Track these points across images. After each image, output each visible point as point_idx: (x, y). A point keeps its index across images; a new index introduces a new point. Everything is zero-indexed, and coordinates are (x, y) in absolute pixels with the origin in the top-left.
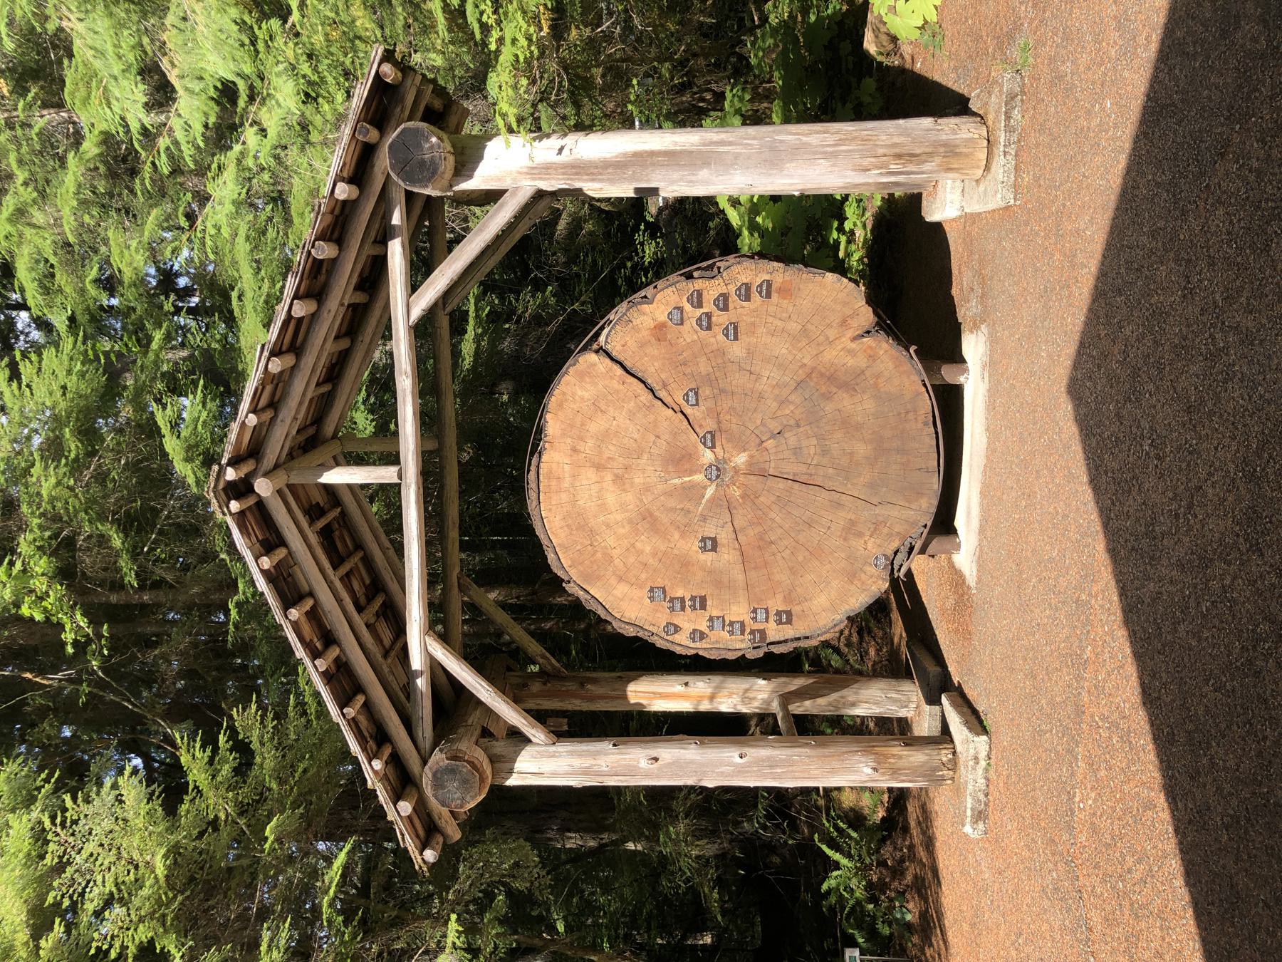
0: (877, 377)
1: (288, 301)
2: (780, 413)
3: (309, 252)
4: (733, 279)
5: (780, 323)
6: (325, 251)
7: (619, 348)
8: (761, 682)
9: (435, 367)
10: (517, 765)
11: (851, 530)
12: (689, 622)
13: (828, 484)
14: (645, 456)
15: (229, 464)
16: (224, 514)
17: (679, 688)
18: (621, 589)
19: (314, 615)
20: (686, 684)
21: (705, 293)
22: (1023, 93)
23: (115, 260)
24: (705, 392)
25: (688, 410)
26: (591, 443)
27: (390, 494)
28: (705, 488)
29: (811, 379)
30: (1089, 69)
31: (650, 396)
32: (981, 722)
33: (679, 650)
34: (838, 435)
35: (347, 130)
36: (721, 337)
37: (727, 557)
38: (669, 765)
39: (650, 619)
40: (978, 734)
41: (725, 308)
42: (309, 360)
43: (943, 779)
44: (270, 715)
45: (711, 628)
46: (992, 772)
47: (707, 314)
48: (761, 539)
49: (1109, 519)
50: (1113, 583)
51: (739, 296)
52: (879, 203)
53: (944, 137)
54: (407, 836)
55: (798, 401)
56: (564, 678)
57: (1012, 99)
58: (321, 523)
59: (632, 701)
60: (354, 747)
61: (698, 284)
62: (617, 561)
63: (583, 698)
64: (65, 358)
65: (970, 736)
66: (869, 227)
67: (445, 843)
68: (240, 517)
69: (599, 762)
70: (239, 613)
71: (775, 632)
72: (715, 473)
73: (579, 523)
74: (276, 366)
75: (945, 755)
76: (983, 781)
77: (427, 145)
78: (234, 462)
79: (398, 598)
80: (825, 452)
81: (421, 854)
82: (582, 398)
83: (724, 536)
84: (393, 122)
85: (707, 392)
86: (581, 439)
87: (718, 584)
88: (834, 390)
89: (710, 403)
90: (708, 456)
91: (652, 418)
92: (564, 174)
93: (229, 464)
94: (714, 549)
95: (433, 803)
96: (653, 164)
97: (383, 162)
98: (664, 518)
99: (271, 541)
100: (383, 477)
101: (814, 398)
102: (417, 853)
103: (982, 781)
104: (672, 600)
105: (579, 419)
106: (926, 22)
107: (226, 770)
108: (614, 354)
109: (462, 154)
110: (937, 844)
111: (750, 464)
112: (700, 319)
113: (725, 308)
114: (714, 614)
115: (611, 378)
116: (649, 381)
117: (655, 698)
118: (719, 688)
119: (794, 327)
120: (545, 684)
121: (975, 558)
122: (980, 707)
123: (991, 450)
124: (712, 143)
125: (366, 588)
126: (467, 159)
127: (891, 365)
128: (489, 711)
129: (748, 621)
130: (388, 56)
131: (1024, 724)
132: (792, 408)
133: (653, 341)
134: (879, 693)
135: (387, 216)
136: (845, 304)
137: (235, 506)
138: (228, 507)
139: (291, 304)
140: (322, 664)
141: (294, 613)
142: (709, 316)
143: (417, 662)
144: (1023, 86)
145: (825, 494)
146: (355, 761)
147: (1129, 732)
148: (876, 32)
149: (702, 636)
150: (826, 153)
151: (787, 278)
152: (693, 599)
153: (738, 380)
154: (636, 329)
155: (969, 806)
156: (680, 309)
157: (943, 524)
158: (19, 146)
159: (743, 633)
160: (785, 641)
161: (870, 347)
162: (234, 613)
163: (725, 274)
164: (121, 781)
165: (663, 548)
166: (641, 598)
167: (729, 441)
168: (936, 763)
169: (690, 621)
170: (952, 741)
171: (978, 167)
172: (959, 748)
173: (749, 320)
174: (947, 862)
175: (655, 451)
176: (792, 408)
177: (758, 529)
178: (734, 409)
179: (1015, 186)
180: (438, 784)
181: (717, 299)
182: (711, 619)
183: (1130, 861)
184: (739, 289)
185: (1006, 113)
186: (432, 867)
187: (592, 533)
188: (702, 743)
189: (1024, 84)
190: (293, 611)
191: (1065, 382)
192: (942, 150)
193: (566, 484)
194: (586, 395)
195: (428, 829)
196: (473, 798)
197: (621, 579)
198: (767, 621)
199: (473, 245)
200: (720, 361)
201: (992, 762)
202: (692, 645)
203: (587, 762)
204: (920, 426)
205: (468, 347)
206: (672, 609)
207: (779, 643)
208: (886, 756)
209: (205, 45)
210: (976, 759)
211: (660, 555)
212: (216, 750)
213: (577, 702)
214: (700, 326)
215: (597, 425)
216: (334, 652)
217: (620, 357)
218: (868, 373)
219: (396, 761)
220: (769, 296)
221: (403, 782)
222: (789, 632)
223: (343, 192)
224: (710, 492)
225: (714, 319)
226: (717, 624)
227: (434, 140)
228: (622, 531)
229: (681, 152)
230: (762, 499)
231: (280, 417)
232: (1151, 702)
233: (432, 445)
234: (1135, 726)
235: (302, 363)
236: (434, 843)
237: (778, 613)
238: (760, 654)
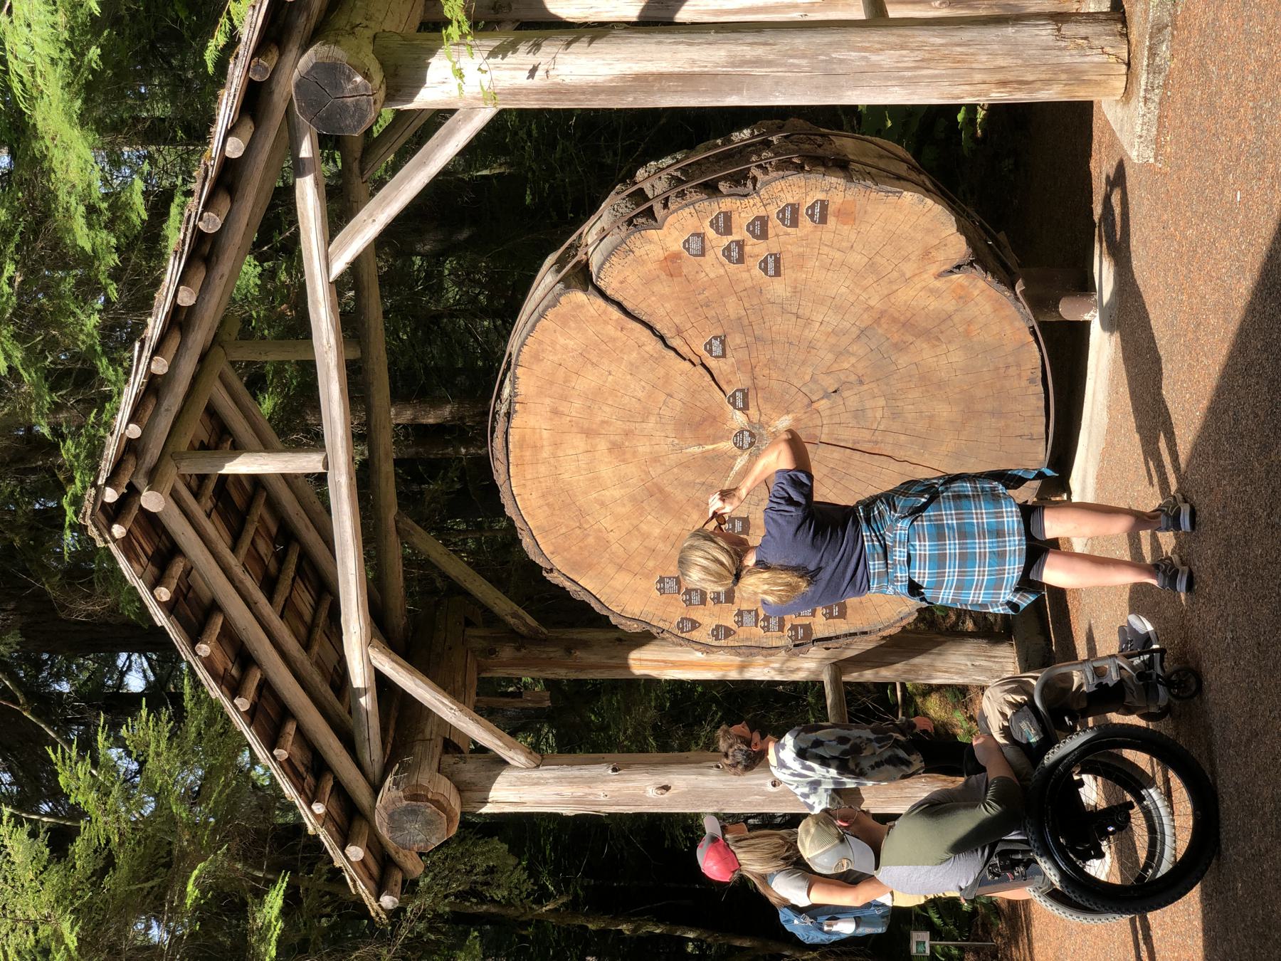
0: (970, 323)
1: (172, 289)
4: (773, 198)
5: (838, 255)
7: (615, 284)
9: (357, 298)
10: (492, 794)
13: (899, 454)
14: (653, 419)
16: (106, 541)
18: (622, 580)
21: (735, 217)
22: (1175, 27)
24: (735, 340)
25: (711, 363)
26: (578, 404)
28: (734, 458)
29: (879, 325)
31: (660, 345)
34: (915, 394)
36: (757, 272)
38: (684, 794)
39: (659, 613)
41: (764, 235)
44: (164, 718)
45: (740, 623)
47: (738, 243)
51: (782, 220)
53: (1068, 60)
54: (359, 882)
55: (861, 352)
56: (545, 641)
57: (1160, 30)
61: (726, 204)
62: (615, 547)
63: (568, 667)
69: (594, 791)
72: (747, 440)
73: (561, 499)
77: (350, 86)
80: (896, 415)
81: (377, 900)
82: (565, 348)
86: (564, 398)
88: (910, 339)
91: (661, 372)
98: (679, 495)
101: (883, 349)
104: (688, 592)
105: (561, 373)
108: (608, 292)
109: (396, 75)
112: (728, 248)
113: (764, 235)
114: (745, 607)
115: (606, 323)
116: (658, 327)
119: (857, 259)
120: (518, 649)
124: (744, 63)
126: (403, 75)
127: (988, 308)
132: (853, 360)
133: (663, 276)
135: (294, 147)
136: (929, 231)
139: (177, 291)
142: (740, 245)
143: (359, 677)
144: (1174, 17)
146: (292, 807)
150: (902, 78)
151: (849, 198)
153: (781, 325)
154: (640, 261)
156: (701, 236)
159: (781, 628)
160: (837, 637)
161: (961, 286)
167: (766, 400)
169: (712, 615)
173: (795, 250)
176: (853, 360)
179: (1156, 141)
181: (753, 223)
184: (783, 211)
185: (1150, 48)
187: (582, 513)
192: (1064, 76)
193: (546, 453)
194: (571, 344)
197: (620, 568)
200: (755, 301)
204: (1024, 383)
206: (689, 603)
211: (673, 538)
214: (729, 257)
215: (587, 381)
218: (956, 318)
220: (823, 220)
221: (350, 818)
223: (237, 148)
225: (747, 249)
226: (748, 619)
228: (621, 510)
229: (701, 74)
235: (190, 343)
236: (391, 884)
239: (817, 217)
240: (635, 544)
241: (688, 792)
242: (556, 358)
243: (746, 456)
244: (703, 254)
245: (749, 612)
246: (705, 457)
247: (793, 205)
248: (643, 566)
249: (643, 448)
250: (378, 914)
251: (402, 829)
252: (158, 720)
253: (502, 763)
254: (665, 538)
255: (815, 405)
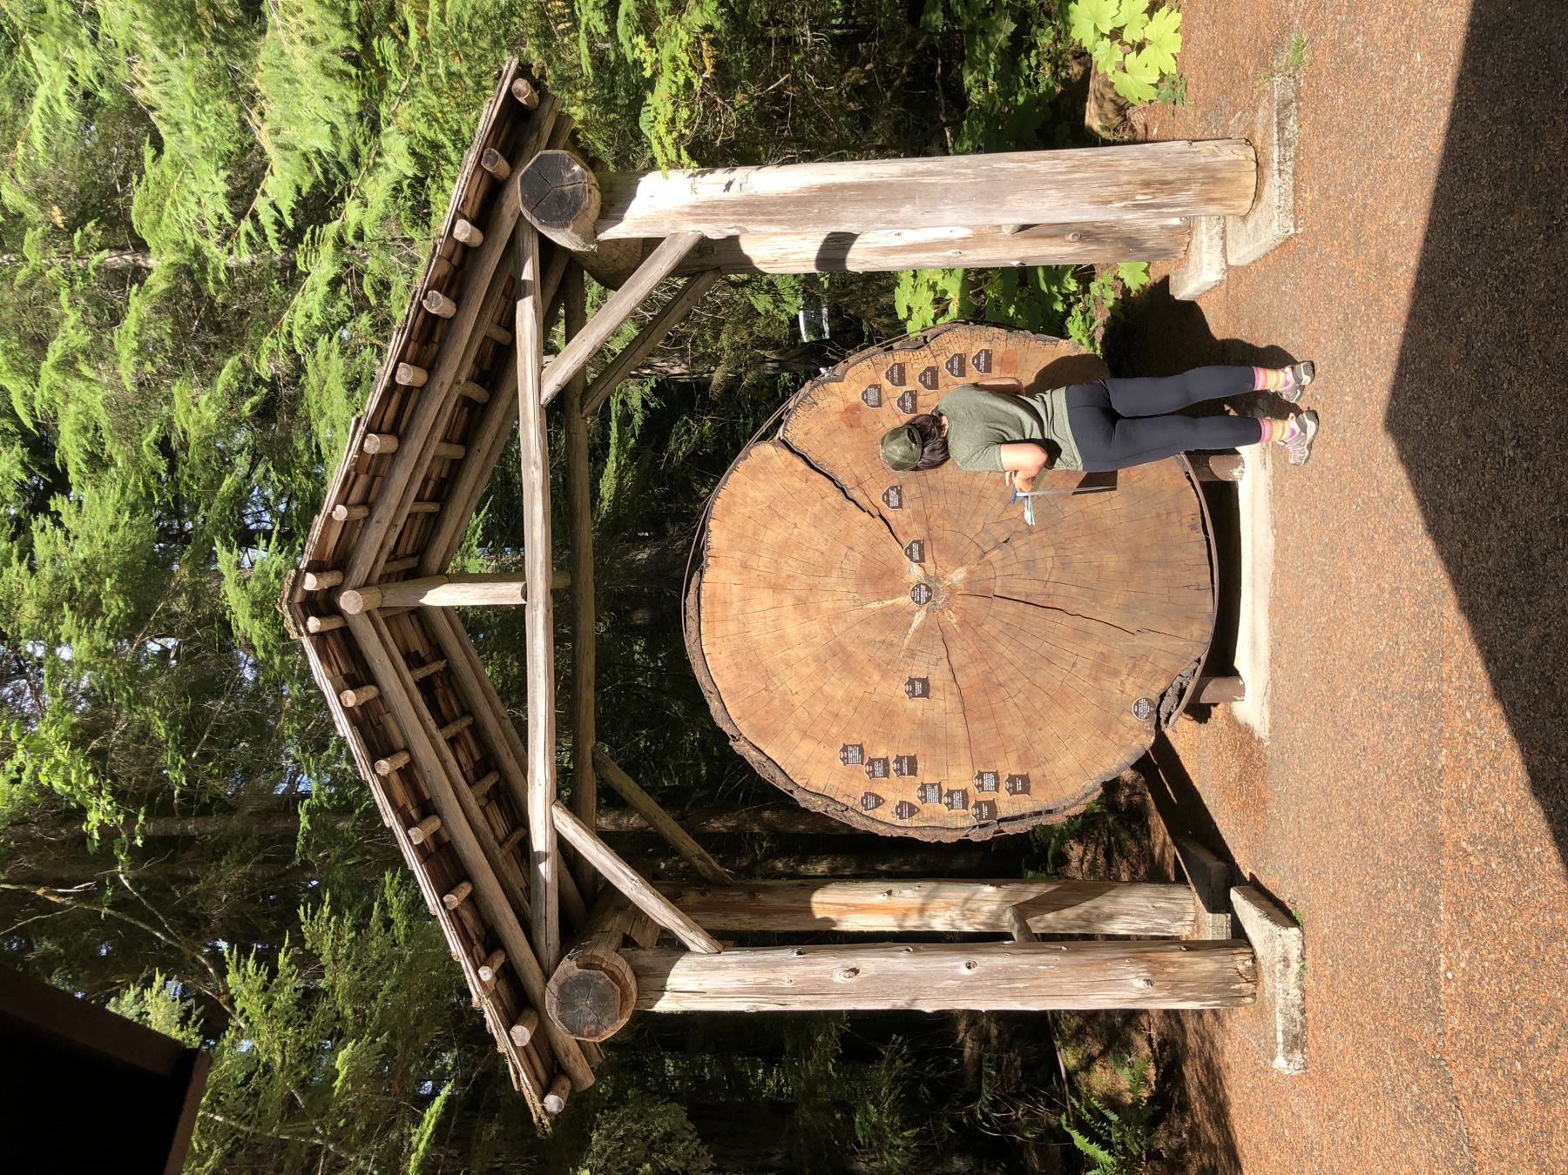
1: (392, 363)
2: (1006, 516)
3: (420, 304)
4: (942, 349)
6: (439, 305)
7: (800, 436)
8: (989, 889)
10: (670, 980)
11: (1103, 666)
12: (895, 791)
13: (1072, 608)
14: (835, 574)
15: (308, 569)
16: (300, 634)
17: (880, 899)
18: (806, 748)
19: (408, 774)
20: (889, 893)
21: (908, 368)
23: (180, 420)
25: (890, 514)
26: (766, 558)
27: (513, 618)
28: (912, 614)
30: (1388, 30)
31: (841, 497)
32: (1288, 913)
33: (882, 831)
34: (1082, 544)
35: (471, 157)
37: (941, 705)
39: (843, 787)
40: (1287, 927)
41: (934, 385)
42: (414, 445)
43: (1240, 995)
44: (348, 923)
45: (924, 799)
46: (1308, 977)
48: (987, 680)
49: (1460, 568)
50: (1474, 650)
51: (951, 370)
52: (1111, 303)
53: (1202, 160)
54: (523, 1075)
56: (730, 887)
58: (422, 673)
59: (818, 916)
60: (456, 948)
61: (899, 357)
63: (753, 912)
64: (111, 510)
65: (1276, 929)
66: (1099, 337)
67: (572, 1090)
68: (320, 639)
69: (780, 975)
70: (310, 821)
71: (1007, 804)
72: (924, 594)
74: (374, 444)
75: (1242, 962)
76: (1297, 992)
78: (316, 567)
79: (515, 775)
80: (1066, 565)
81: (542, 1100)
82: (755, 501)
83: (939, 676)
84: (527, 153)
85: (913, 491)
87: (931, 740)
89: (917, 505)
90: (915, 572)
91: (842, 524)
92: (734, 214)
93: (308, 569)
94: (925, 693)
95: (558, 1029)
96: (844, 200)
97: (514, 200)
98: (861, 655)
99: (357, 673)
100: (503, 596)
102: (536, 1099)
103: (1295, 992)
104: (871, 762)
106: (1162, 75)
107: (283, 999)
110: (1233, 1111)
111: (969, 581)
112: (902, 399)
113: (934, 385)
114: (928, 780)
116: (840, 478)
117: (849, 912)
118: (931, 896)
120: (703, 894)
121: (1267, 699)
122: (1284, 897)
123: (1281, 548)
124: (916, 173)
125: (475, 763)
126: (614, 202)
128: (637, 914)
129: (972, 790)
130: (524, 71)
131: (1353, 892)
133: (844, 428)
134: (1144, 902)
137: (314, 624)
138: (305, 625)
140: (418, 836)
141: (384, 766)
142: (914, 395)
143: (540, 841)
145: (1067, 620)
147: (1516, 843)
148: (1101, 98)
149: (913, 810)
151: (1011, 347)
152: (899, 760)
154: (823, 413)
155: (1280, 1028)
157: (1220, 662)
158: (72, 282)
159: (965, 806)
160: (1022, 817)
162: (304, 822)
163: (932, 343)
164: (147, 994)
165: (859, 693)
166: (832, 760)
168: (1231, 973)
169: (896, 790)
170: (1249, 945)
171: (1246, 196)
172: (1260, 950)
174: (1248, 1133)
175: (848, 566)
177: (983, 667)
178: (948, 511)
180: (566, 1001)
181: (924, 374)
182: (923, 788)
183: (1530, 1027)
184: (951, 361)
186: (556, 1119)
187: (768, 675)
188: (916, 950)
189: (1299, 89)
190: (383, 762)
191: (1380, 419)
192: (1200, 175)
193: (735, 610)
194: (760, 496)
195: (552, 1071)
196: (612, 1021)
197: (805, 734)
198: (997, 790)
199: (621, 305)
201: (1307, 963)
202: (899, 823)
203: (762, 977)
204: (1186, 530)
205: (607, 486)
206: (872, 774)
207: (1013, 819)
208: (1163, 965)
209: (302, 109)
210: (1286, 961)
211: (855, 701)
212: (273, 972)
213: (746, 917)
215: (772, 536)
216: (433, 824)
217: (803, 449)
219: (509, 975)
222: (1026, 804)
223: (465, 231)
224: (918, 619)
225: (920, 399)
226: (932, 794)
227: (577, 168)
228: (806, 671)
230: (986, 627)
231: (376, 516)
232: (1546, 790)
233: (563, 581)
234: (1524, 832)
236: (558, 1087)
237: (1012, 779)
238: (988, 835)
239: (982, 366)
240: (819, 708)
241: (878, 977)
242: (746, 511)
243: (923, 612)
244: (880, 405)
245: (933, 785)
246: (884, 613)
247: (960, 355)
248: (826, 734)
249: (827, 604)
250: (540, 1120)
251: (572, 1006)
252: (339, 924)
253: (683, 949)
254: (848, 702)
255: (988, 557)
